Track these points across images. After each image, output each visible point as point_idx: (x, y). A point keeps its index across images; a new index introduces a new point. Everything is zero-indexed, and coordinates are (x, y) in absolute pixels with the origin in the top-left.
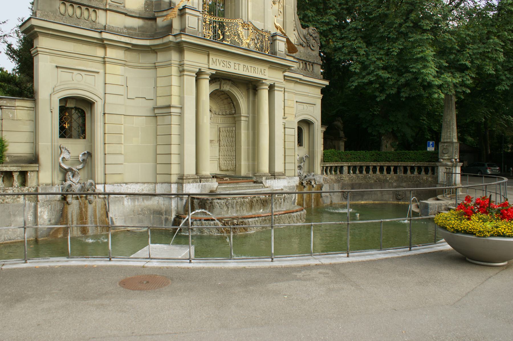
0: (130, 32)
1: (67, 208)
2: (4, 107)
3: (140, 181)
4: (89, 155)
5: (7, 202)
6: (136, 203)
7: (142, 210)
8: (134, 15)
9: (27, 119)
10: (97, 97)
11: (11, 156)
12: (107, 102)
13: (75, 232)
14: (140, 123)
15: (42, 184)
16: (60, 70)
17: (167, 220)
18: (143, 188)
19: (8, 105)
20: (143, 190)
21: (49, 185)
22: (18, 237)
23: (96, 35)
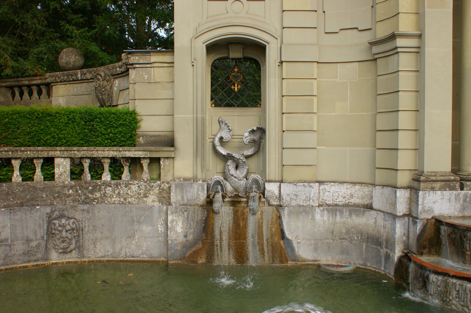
1: (213, 219)
2: (137, 66)
3: (348, 180)
4: (262, 131)
5: (129, 203)
6: (338, 218)
7: (348, 232)
9: (168, 81)
10: (269, 36)
11: (147, 136)
12: (284, 41)
13: (225, 257)
14: (349, 74)
15: (179, 178)
17: (388, 257)
18: (353, 192)
19: (141, 61)
20: (352, 196)
21: (189, 180)
22: (143, 254)
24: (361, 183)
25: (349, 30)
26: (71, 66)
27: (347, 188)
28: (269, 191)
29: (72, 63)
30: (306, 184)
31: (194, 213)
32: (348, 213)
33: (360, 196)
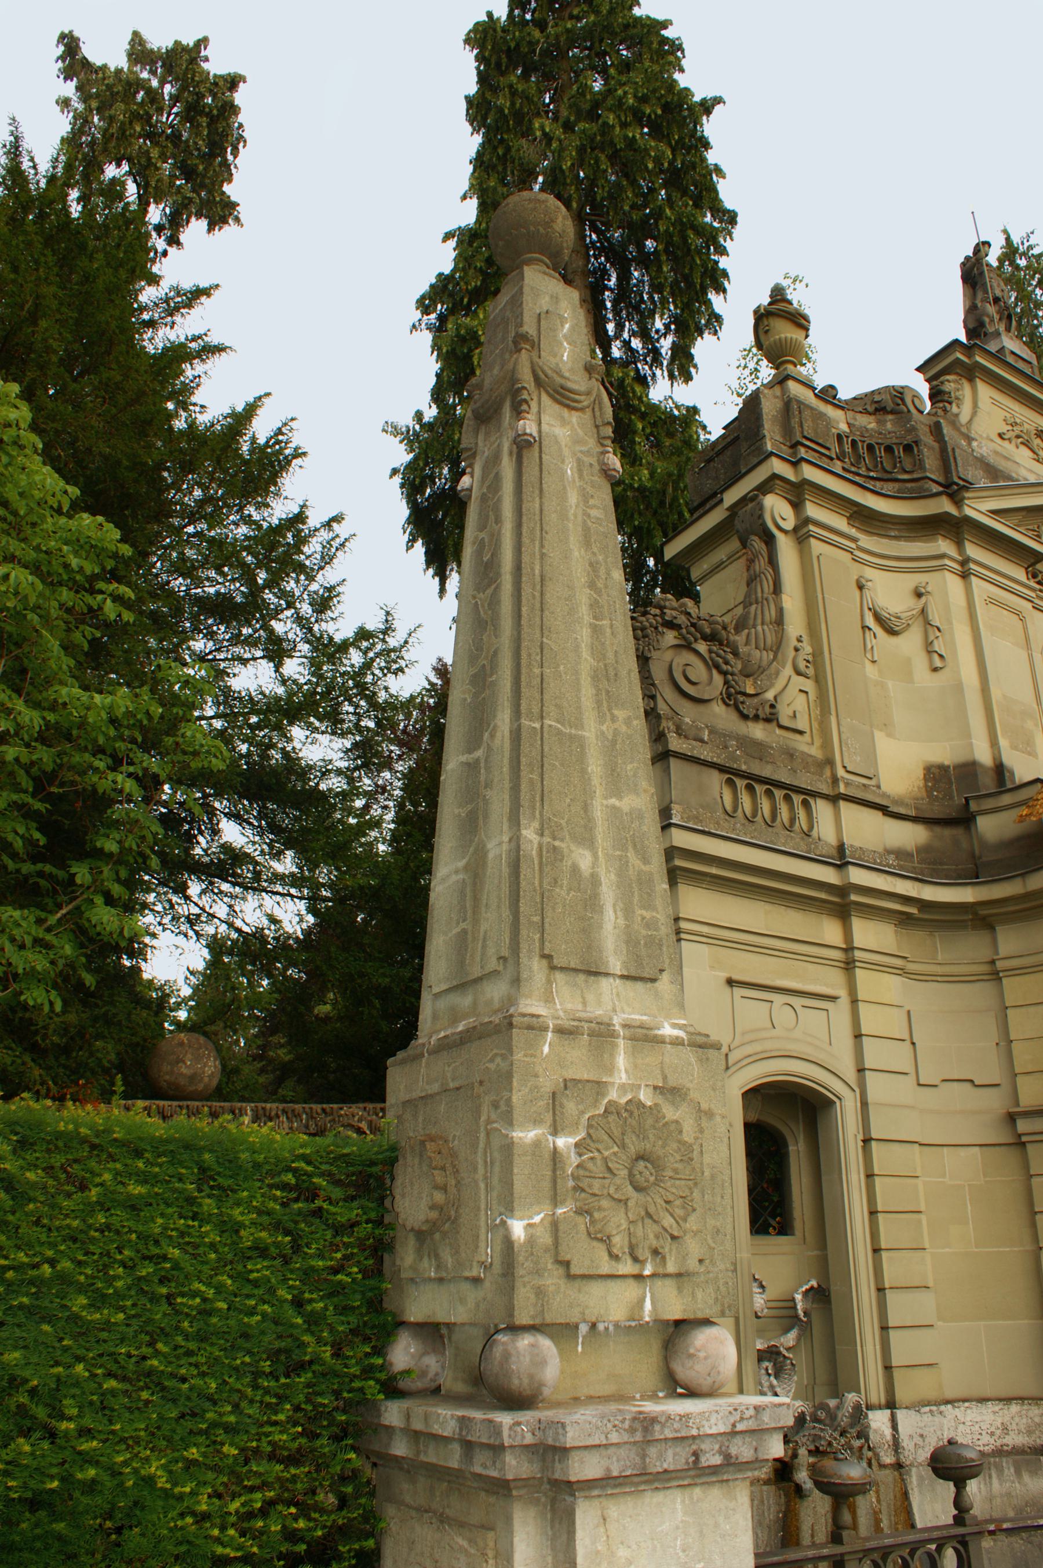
0: (900, 862)
3: (989, 1394)
8: (902, 810)
12: (871, 1098)
16: (739, 992)
18: (1007, 1419)
20: (1005, 1429)
23: (828, 875)
24: (1021, 1399)
25: (955, 1084)
26: (200, 1087)
27: (994, 1413)
28: (875, 1431)
29: (206, 1079)
30: (934, 1408)
31: (762, 1502)
32: (1012, 1470)
33: (1022, 1427)
